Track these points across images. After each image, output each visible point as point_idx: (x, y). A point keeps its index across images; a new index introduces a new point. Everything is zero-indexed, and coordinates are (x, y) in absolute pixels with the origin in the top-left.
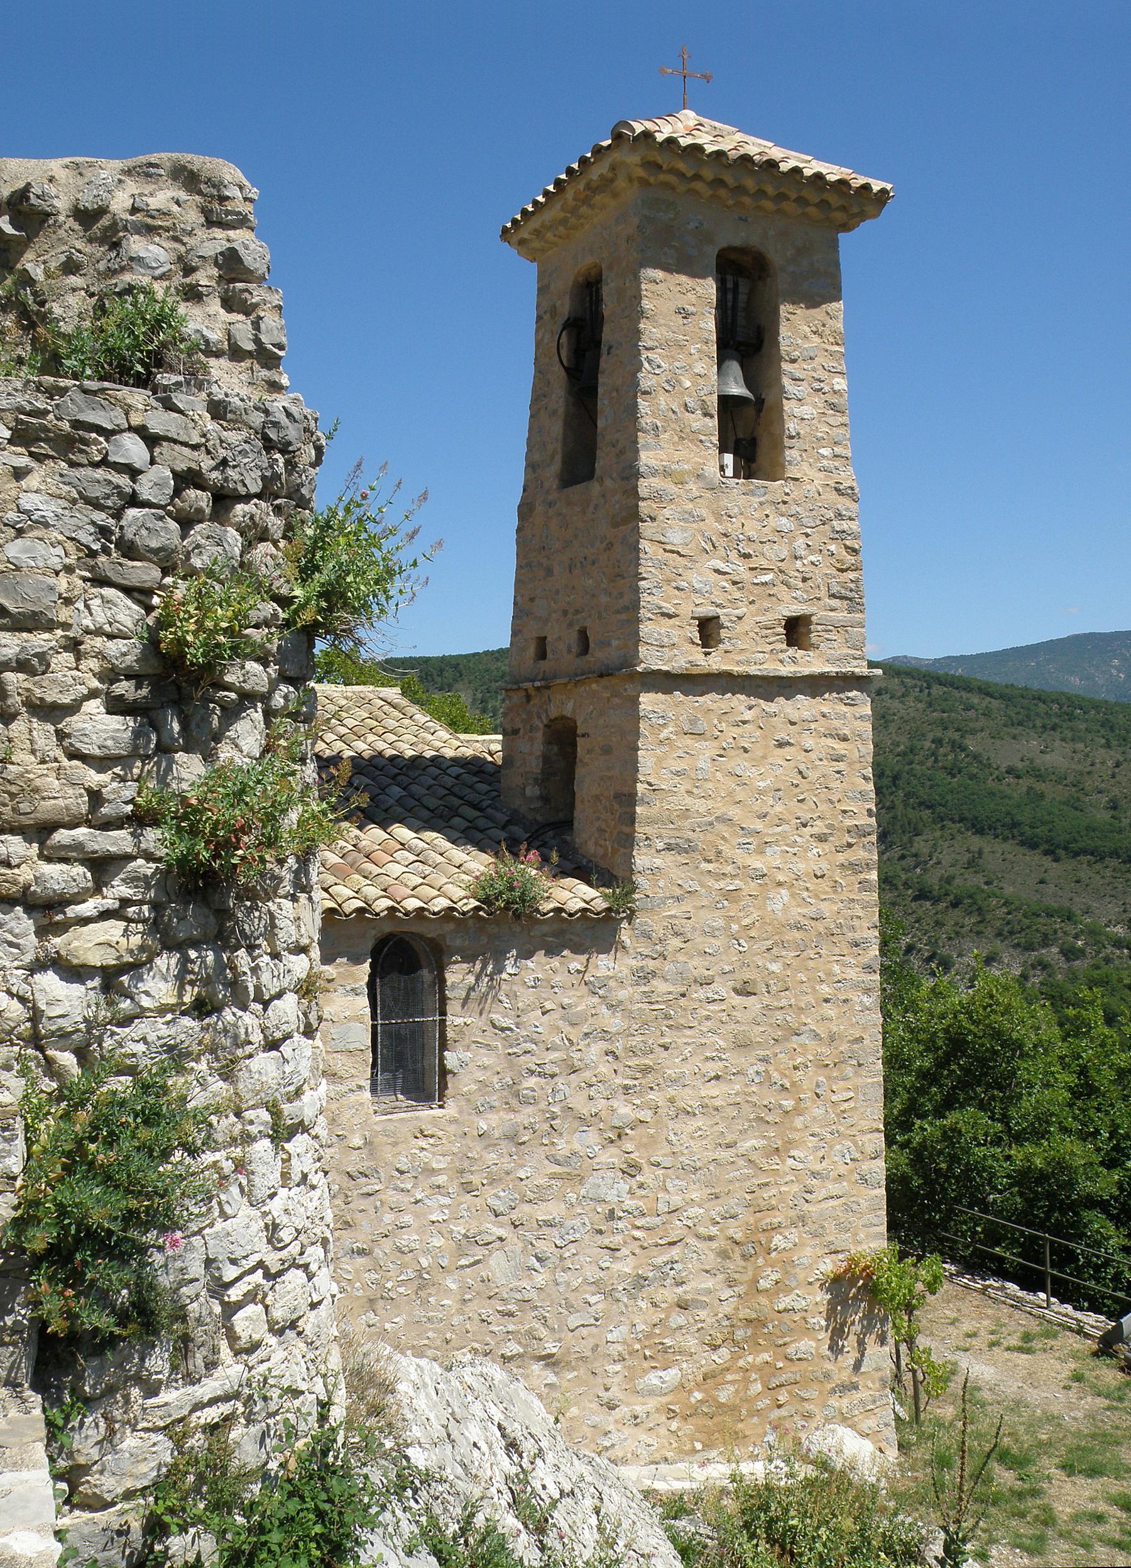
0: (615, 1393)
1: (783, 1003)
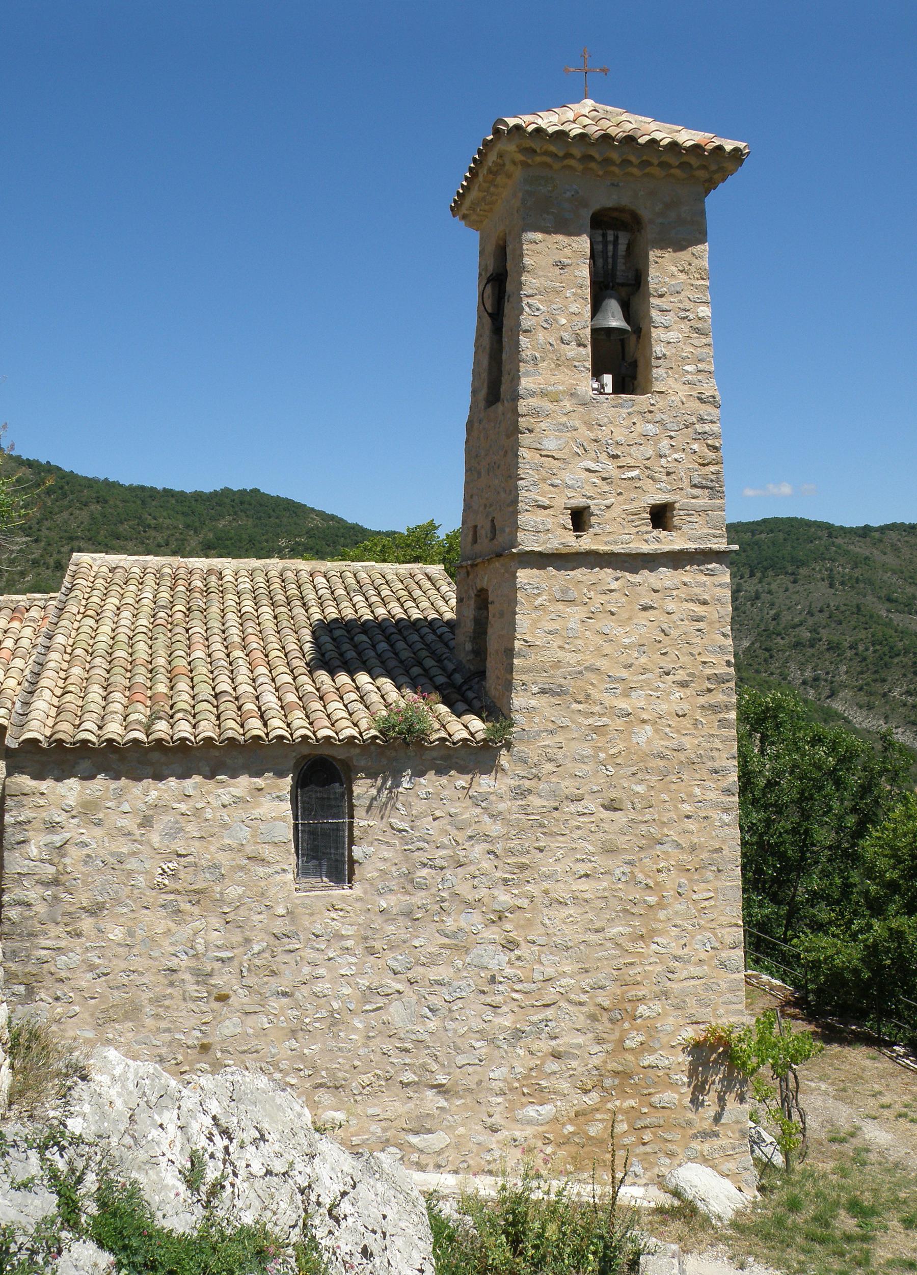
0: (497, 1119)
1: (647, 817)
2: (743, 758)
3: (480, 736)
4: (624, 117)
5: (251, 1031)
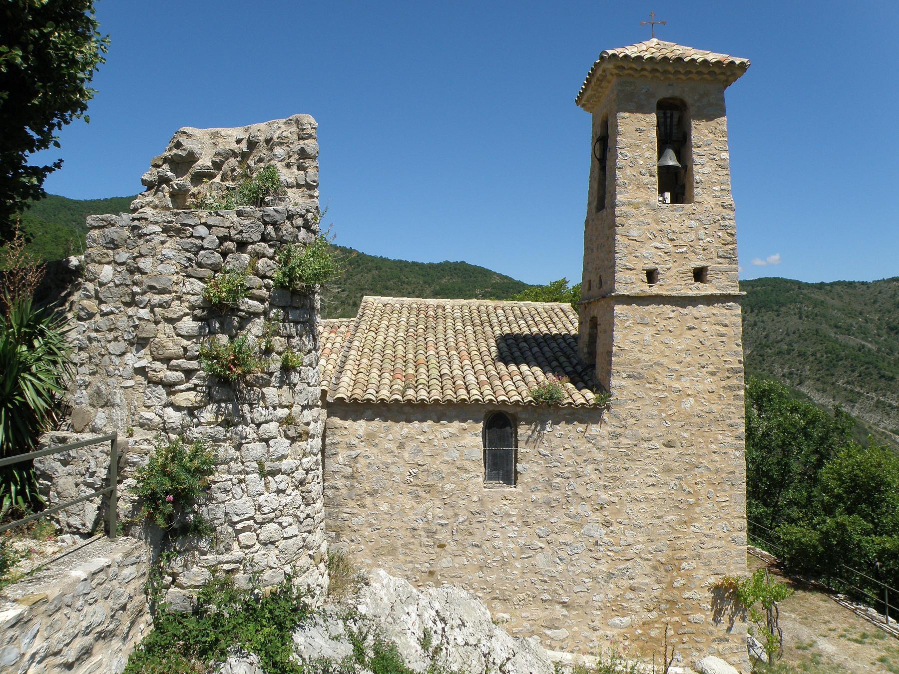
0: (597, 624)
1: (690, 452)
2: (748, 419)
3: (592, 402)
4: (675, 48)
5: (457, 565)
